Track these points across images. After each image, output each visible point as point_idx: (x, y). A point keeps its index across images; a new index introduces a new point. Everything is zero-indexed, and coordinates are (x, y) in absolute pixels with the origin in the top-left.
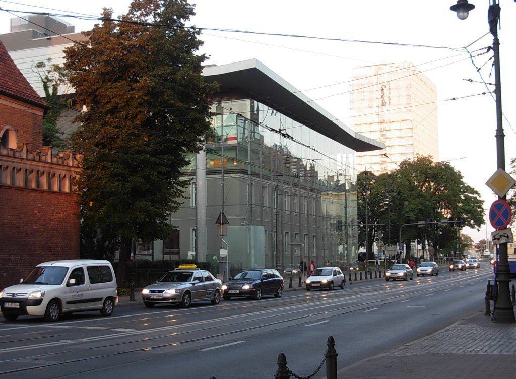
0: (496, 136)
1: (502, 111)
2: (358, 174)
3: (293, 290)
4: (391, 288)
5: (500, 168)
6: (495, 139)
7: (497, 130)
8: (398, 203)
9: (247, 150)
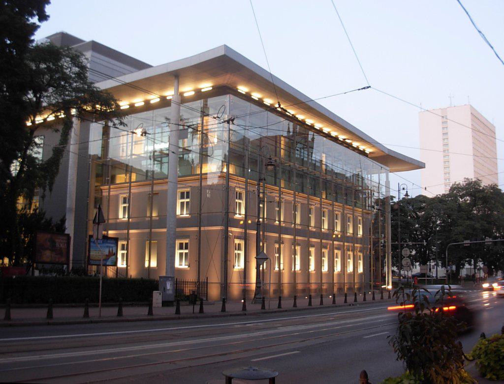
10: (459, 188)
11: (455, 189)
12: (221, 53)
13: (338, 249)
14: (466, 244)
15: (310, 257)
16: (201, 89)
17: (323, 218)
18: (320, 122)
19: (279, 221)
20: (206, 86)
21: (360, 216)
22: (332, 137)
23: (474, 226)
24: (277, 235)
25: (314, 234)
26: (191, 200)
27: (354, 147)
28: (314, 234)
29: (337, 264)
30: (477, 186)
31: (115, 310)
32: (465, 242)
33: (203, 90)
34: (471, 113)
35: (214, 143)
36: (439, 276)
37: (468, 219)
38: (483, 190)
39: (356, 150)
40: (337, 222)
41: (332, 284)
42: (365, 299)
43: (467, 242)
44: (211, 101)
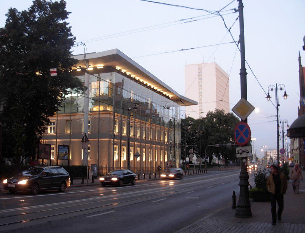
0: (240, 74)
1: (246, 59)
2: (184, 118)
3: (95, 185)
4: (105, 194)
5: (243, 98)
6: (239, 76)
7: (241, 70)
8: (206, 135)
9: (113, 99)
10: (212, 114)
11: (210, 114)
12: (115, 53)
13: (138, 147)
14: (217, 146)
15: (115, 151)
16: (97, 67)
17: (115, 125)
18: (160, 88)
19: (156, 139)
20: (100, 66)
21: (139, 124)
22: (136, 80)
23: (220, 136)
24: (150, 145)
25: (147, 142)
26: (91, 125)
27: (127, 75)
28: (147, 142)
29: (124, 155)
30: (222, 114)
31: (80, 181)
32: (216, 145)
33: (98, 68)
34: (216, 68)
35: (294, 164)
36: (220, 164)
37: (217, 132)
38: (225, 116)
39: (165, 96)
40: (124, 128)
41: (152, 168)
42: (150, 178)
43: (217, 145)
44: (102, 75)
